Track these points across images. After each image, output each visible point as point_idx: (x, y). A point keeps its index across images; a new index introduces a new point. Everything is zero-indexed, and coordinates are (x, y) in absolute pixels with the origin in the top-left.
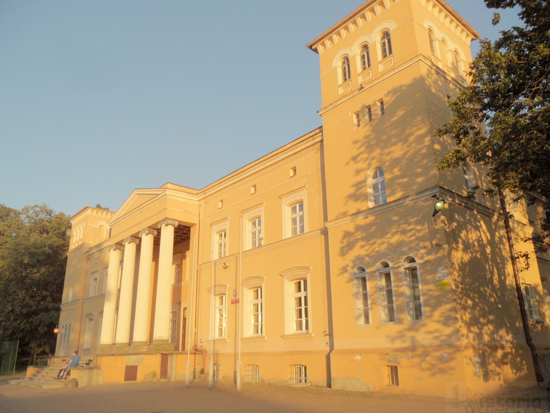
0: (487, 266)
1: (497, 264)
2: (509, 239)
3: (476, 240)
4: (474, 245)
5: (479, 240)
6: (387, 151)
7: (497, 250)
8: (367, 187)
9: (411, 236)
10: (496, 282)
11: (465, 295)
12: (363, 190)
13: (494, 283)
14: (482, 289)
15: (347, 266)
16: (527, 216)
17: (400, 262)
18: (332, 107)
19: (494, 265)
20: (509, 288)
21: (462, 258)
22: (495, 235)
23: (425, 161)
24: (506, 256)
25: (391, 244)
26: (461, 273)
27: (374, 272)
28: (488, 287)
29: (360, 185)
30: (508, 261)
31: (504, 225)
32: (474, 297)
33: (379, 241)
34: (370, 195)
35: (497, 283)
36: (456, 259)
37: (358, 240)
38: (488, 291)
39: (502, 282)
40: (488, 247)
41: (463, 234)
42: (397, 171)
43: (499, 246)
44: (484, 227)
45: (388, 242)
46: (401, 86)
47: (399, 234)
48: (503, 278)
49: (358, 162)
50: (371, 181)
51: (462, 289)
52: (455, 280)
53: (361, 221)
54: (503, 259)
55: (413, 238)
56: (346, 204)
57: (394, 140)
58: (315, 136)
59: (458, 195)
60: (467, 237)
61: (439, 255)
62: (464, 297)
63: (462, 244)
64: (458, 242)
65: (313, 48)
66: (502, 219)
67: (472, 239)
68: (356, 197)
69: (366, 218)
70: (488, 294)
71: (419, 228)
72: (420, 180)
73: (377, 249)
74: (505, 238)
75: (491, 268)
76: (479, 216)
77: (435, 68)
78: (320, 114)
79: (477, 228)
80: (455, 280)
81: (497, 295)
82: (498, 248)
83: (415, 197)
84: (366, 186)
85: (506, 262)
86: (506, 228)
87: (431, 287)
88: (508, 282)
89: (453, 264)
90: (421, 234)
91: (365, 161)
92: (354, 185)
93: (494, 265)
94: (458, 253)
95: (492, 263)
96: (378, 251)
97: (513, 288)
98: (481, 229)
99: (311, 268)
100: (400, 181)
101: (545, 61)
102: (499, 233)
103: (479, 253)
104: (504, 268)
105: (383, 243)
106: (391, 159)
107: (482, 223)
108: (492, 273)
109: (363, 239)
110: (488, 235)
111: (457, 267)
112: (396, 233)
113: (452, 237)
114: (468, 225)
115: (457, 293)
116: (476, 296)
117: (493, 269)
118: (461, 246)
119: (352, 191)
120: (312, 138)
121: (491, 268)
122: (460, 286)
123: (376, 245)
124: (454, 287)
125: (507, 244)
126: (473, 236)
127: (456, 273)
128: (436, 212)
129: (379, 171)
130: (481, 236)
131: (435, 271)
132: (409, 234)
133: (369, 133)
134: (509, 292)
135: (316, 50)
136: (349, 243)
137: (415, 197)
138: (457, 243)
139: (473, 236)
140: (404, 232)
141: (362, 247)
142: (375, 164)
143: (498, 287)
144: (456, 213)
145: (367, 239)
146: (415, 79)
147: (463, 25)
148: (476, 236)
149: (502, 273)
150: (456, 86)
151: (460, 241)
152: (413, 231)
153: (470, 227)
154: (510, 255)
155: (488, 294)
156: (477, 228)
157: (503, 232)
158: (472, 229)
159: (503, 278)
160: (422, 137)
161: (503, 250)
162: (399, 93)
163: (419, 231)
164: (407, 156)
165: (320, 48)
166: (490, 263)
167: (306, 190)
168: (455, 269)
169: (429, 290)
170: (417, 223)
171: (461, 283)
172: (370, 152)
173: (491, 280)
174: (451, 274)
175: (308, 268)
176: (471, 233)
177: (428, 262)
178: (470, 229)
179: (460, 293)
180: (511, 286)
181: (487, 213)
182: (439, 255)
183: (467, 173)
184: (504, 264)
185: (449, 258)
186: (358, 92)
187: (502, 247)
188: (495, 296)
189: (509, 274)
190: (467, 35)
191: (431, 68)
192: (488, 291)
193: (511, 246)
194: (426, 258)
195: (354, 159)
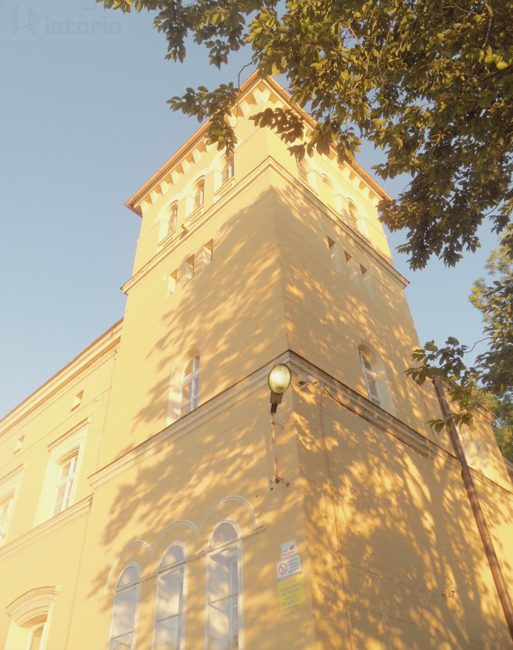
0: (427, 559)
1: (454, 563)
2: (476, 509)
3: (393, 491)
4: (388, 503)
5: (402, 494)
6: (210, 314)
7: (450, 529)
8: (170, 389)
9: (234, 472)
10: (452, 602)
11: (355, 623)
12: (163, 396)
13: (449, 606)
14: (414, 615)
15: (108, 569)
16: (509, 478)
17: (206, 541)
18: (141, 275)
19: (444, 558)
20: (490, 622)
21: (353, 522)
22: (444, 495)
23: (270, 312)
24: (473, 546)
25: (196, 498)
26: (345, 561)
27: (154, 576)
28: (434, 615)
29: (160, 388)
30: (480, 558)
31: (461, 480)
32: (388, 633)
33: (175, 497)
34: (175, 405)
35: (458, 607)
36: (331, 521)
37: (137, 503)
38: (434, 623)
39: (472, 607)
40: (427, 515)
41: (357, 469)
42: (221, 345)
43: (455, 520)
44: (413, 470)
45: (190, 495)
46: (242, 211)
47: (211, 473)
48: (471, 595)
49: (166, 347)
50: (180, 379)
51: (346, 603)
52: (327, 576)
53: (151, 459)
54: (468, 552)
55: (237, 476)
56: (133, 431)
57: (223, 294)
58: (115, 330)
59: (345, 387)
60: (367, 479)
61: (285, 508)
62: (356, 631)
63: (353, 491)
64: (343, 484)
65: (135, 207)
66: (456, 467)
67: (382, 486)
68: (149, 413)
69: (159, 451)
70: (433, 632)
71: (249, 450)
72: (260, 348)
73: (168, 517)
74: (467, 507)
75: (438, 565)
76: (400, 446)
77: (301, 189)
78: (124, 291)
79: (398, 469)
80: (327, 576)
81: (459, 637)
82: (452, 523)
83: (247, 383)
84: (168, 387)
85: (475, 559)
86: (467, 487)
87: (266, 598)
88: (485, 608)
89: (321, 531)
90: (252, 464)
91: (175, 343)
92: (152, 391)
93: (444, 558)
94: (340, 509)
95: (440, 554)
96: (170, 521)
97: (502, 624)
98: (405, 473)
99: (58, 588)
100: (226, 360)
101: (510, 324)
102: (453, 495)
103: (403, 524)
104: (473, 574)
105: (179, 502)
106: (216, 325)
107: (408, 461)
108: (442, 579)
109: (146, 499)
110: (426, 489)
111: (335, 541)
112: (205, 472)
113: (325, 471)
114: (370, 456)
115: (332, 614)
116: (397, 631)
117: (443, 568)
118: (348, 494)
119: (146, 401)
120: (109, 335)
121: (438, 565)
122: (342, 595)
123: (168, 508)
124: (319, 596)
125: (473, 521)
126: (385, 482)
127: (329, 558)
128: (276, 398)
129: (195, 355)
130: (406, 487)
131: (273, 555)
132: (231, 469)
133: (188, 294)
134: (491, 634)
135: (139, 212)
136: (122, 513)
137: (247, 383)
138: (338, 484)
139: (385, 482)
140: (221, 466)
141: (143, 517)
142: (190, 342)
143: (459, 615)
144: (338, 420)
145: (151, 497)
146: (262, 194)
147: (362, 176)
148: (395, 484)
149: (468, 584)
150: (347, 234)
151: (347, 481)
152: (238, 461)
153: (377, 460)
154: (482, 544)
155: (433, 632)
156: (398, 469)
157: (460, 494)
158: (383, 465)
159: (297, 301)
160: (269, 270)
161: (465, 532)
162: (238, 222)
163: (249, 457)
164: (240, 315)
165: (144, 206)
166: (435, 553)
167: (88, 426)
168: (329, 546)
169: (264, 609)
170: (246, 441)
171: (346, 590)
172: (184, 326)
173: (440, 595)
174: (314, 558)
175: (50, 590)
176: (379, 474)
177: (262, 529)
178: (378, 465)
179: (340, 616)
180: (495, 619)
181: (423, 450)
182: (285, 508)
183: (372, 367)
184: (472, 565)
185: (309, 514)
186: (180, 241)
187: (462, 524)
188: (454, 639)
189: (486, 591)
190: (371, 195)
191: (294, 187)
192: (434, 623)
193: (482, 525)
194: (257, 522)
195: (160, 345)
